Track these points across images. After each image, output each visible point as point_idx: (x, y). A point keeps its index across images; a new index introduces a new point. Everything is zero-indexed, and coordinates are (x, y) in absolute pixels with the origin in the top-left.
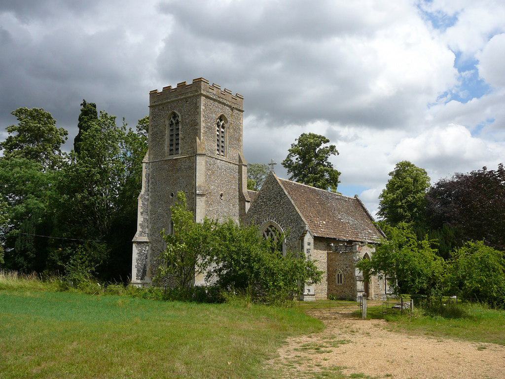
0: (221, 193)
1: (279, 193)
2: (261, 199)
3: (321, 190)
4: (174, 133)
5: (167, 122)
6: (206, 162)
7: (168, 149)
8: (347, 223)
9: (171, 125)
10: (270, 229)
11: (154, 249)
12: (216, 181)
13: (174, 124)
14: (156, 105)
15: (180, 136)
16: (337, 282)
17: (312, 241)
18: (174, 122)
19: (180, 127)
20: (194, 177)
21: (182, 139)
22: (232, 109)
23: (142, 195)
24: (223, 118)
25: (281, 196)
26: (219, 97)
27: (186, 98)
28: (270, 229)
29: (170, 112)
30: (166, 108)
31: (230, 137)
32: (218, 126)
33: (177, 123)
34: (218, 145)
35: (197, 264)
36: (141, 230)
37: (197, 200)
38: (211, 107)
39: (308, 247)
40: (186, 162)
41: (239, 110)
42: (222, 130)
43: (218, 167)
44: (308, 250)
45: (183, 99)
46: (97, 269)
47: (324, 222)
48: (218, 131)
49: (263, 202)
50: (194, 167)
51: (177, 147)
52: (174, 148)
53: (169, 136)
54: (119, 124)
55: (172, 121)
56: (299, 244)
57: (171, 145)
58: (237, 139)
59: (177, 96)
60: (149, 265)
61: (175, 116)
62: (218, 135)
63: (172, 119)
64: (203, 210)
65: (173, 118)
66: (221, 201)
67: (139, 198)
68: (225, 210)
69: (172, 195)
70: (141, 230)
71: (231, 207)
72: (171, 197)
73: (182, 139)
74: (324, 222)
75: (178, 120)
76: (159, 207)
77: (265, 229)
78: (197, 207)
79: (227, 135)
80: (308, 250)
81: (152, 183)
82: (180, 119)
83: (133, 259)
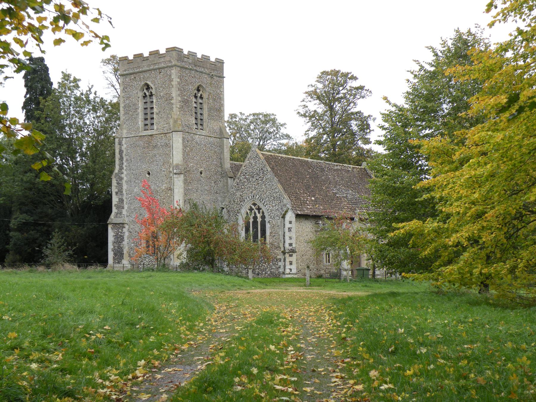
0: (200, 170)
1: (262, 169)
2: (244, 175)
3: (315, 161)
4: (149, 111)
5: (141, 94)
6: (184, 139)
7: (143, 123)
8: (344, 197)
9: (145, 96)
10: (253, 207)
11: (132, 231)
12: (195, 158)
13: (148, 96)
14: (127, 74)
15: (155, 110)
16: (325, 262)
17: (293, 219)
18: (147, 94)
19: (154, 101)
20: (171, 155)
21: (157, 114)
22: (212, 77)
23: (116, 173)
24: (201, 89)
25: (263, 173)
26: (195, 66)
27: (159, 69)
28: (253, 207)
29: (143, 83)
30: (138, 78)
31: (210, 109)
32: (196, 97)
33: (151, 95)
34: (196, 119)
35: (26, 148)
36: (116, 211)
37: (175, 179)
38: (187, 78)
39: (290, 226)
40: (162, 139)
41: (219, 77)
42: (200, 101)
43: (197, 143)
44: (289, 228)
45: (156, 69)
46: (76, 252)
47: (313, 198)
48: (195, 102)
49: (245, 178)
50: (171, 144)
51: (152, 122)
52: (148, 122)
53: (143, 109)
54: (83, 87)
55: (145, 94)
56: (281, 222)
57: (146, 119)
58: (219, 109)
59: (149, 65)
60: (127, 248)
61: (148, 87)
62: (195, 107)
63: (145, 91)
64: (182, 190)
65: (147, 89)
66: (202, 179)
67: (113, 177)
68: (206, 188)
69: (149, 174)
70: (116, 211)
71: (213, 184)
72: (147, 176)
73: (157, 114)
74: (313, 198)
75: (151, 93)
76: (135, 186)
77: (248, 207)
78: (175, 187)
79: (205, 106)
80: (289, 228)
81: (127, 160)
82: (153, 92)
83: (109, 244)
